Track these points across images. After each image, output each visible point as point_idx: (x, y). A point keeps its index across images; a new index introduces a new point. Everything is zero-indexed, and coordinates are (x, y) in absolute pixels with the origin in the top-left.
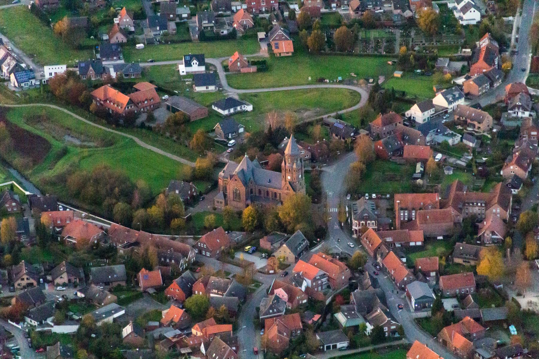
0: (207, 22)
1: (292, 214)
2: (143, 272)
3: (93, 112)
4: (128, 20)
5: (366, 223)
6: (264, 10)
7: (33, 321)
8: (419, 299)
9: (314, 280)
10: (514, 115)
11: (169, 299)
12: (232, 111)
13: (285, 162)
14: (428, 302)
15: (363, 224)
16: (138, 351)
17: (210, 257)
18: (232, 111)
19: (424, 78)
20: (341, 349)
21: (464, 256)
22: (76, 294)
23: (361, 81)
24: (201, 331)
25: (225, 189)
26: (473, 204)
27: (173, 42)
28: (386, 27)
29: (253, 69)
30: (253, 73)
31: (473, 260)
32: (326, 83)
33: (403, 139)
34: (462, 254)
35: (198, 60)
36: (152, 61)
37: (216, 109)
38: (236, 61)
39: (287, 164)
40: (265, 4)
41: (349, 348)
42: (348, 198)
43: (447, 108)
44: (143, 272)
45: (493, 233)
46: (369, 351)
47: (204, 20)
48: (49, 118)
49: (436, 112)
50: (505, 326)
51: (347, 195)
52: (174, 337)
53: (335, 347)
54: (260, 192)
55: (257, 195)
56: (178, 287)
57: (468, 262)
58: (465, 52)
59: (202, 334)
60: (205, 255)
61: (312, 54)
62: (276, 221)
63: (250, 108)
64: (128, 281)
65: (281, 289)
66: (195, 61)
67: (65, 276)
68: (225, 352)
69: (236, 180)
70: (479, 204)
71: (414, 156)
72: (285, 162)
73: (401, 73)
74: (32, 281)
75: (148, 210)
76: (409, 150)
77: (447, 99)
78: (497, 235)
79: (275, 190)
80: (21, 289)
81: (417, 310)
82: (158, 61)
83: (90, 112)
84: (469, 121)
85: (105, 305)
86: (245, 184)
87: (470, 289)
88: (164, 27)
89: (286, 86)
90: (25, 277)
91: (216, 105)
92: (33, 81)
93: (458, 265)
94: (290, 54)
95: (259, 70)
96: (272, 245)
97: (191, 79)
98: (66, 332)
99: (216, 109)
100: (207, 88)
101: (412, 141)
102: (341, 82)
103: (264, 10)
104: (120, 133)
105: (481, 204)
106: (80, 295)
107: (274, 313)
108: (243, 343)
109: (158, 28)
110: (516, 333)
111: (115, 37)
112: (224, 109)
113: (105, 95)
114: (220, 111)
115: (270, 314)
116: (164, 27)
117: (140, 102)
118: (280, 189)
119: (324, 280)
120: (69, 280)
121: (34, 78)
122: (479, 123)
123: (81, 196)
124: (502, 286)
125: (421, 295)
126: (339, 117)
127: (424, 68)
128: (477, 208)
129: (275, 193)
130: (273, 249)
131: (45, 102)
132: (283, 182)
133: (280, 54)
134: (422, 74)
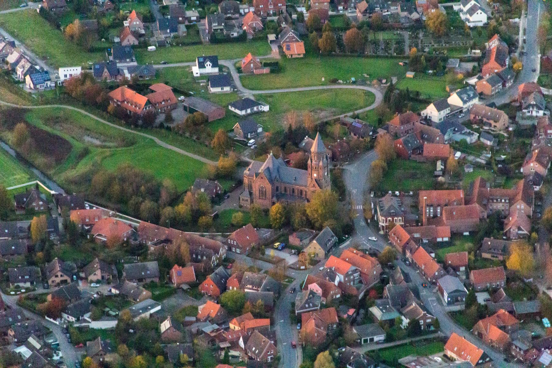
1: (320, 212)
3: (112, 113)
6: (271, 12)
7: (70, 317)
8: (451, 293)
9: (347, 275)
12: (249, 111)
13: (311, 160)
15: (389, 220)
18: (249, 111)
20: (378, 343)
22: (110, 291)
23: (375, 81)
24: (240, 326)
26: (497, 200)
27: (184, 44)
28: (394, 28)
29: (266, 70)
30: (267, 74)
31: (501, 254)
32: (340, 84)
33: (422, 138)
35: (211, 62)
36: (165, 63)
37: (233, 109)
39: (314, 162)
40: (272, 7)
41: (387, 341)
42: (372, 196)
43: (462, 108)
45: (519, 229)
47: (214, 22)
49: (451, 111)
50: (538, 319)
52: (213, 332)
53: (372, 340)
54: (285, 190)
57: (498, 257)
58: (475, 53)
59: (240, 328)
63: (266, 108)
64: (161, 277)
65: (315, 284)
66: (208, 63)
67: (99, 272)
69: (262, 178)
70: (503, 201)
71: (433, 154)
73: (413, 73)
74: (65, 278)
77: (462, 99)
78: (523, 230)
79: (302, 188)
81: (449, 303)
84: (485, 120)
85: (140, 301)
86: (271, 181)
87: (500, 282)
88: (174, 29)
90: (59, 274)
92: (49, 83)
93: (486, 260)
94: (302, 56)
95: (272, 72)
96: (301, 241)
98: (103, 328)
99: (233, 109)
102: (354, 83)
105: (505, 201)
107: (309, 307)
109: (168, 31)
112: (241, 110)
114: (238, 111)
115: (306, 308)
118: (306, 186)
119: (356, 275)
122: (495, 122)
126: (356, 117)
127: (435, 69)
128: (501, 204)
130: (302, 245)
131: (61, 104)
133: (292, 55)
134: (434, 74)
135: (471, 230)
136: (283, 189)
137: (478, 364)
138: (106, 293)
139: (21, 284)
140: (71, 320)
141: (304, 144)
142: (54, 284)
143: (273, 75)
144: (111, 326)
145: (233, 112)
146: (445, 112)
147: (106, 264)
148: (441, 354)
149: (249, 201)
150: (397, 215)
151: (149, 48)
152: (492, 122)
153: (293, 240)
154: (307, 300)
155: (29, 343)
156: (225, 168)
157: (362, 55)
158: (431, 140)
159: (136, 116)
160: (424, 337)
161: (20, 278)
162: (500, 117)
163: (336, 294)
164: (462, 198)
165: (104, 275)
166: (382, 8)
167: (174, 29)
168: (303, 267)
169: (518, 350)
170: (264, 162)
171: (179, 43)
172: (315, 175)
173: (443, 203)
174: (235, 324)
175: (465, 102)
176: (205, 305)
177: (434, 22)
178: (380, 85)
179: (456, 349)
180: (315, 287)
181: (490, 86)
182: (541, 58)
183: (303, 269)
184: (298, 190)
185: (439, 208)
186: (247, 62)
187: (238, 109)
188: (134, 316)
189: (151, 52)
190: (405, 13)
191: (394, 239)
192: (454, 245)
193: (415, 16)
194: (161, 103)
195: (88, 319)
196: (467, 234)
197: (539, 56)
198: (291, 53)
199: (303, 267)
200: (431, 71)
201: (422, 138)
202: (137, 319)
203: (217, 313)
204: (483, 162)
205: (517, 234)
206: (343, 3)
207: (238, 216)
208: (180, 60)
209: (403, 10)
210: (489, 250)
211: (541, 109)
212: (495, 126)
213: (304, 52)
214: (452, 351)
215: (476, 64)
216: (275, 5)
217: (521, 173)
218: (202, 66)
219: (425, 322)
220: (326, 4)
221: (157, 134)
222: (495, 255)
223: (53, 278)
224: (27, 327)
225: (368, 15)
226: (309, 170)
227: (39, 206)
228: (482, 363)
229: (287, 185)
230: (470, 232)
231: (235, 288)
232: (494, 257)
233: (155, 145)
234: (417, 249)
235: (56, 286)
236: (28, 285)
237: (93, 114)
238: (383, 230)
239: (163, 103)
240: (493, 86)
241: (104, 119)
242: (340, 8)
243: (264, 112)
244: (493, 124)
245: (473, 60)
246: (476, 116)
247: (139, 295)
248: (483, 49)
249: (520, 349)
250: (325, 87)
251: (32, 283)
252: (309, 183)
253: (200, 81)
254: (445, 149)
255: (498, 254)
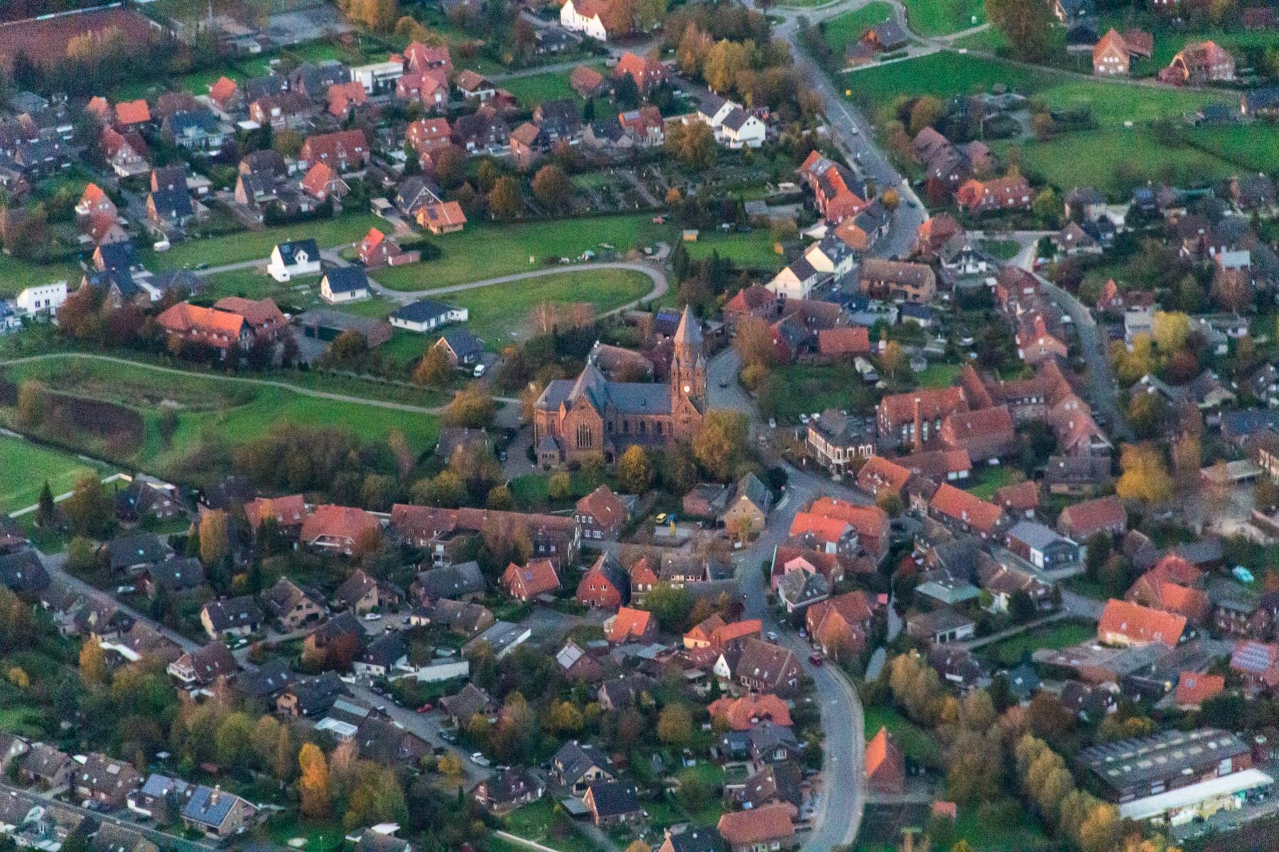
1: (726, 447)
2: (513, 571)
5: (857, 449)
6: (343, 166)
7: (374, 667)
12: (433, 323)
13: (678, 362)
17: (603, 539)
18: (433, 323)
20: (965, 639)
21: (1071, 478)
24: (708, 638)
26: (1022, 400)
28: (598, 168)
29: (413, 257)
30: (413, 264)
32: (563, 264)
34: (1066, 475)
35: (307, 251)
36: (205, 267)
37: (400, 323)
39: (682, 363)
40: (345, 155)
43: (832, 274)
44: (513, 571)
47: (257, 189)
48: (88, 374)
49: (819, 281)
50: (1223, 569)
53: (953, 636)
55: (621, 432)
59: (708, 644)
61: (506, 220)
62: (693, 466)
63: (462, 315)
66: (302, 253)
67: (374, 593)
68: (781, 660)
69: (582, 408)
70: (1034, 400)
72: (678, 362)
73: (696, 232)
74: (315, 609)
82: (215, 265)
84: (893, 286)
86: (601, 410)
88: (185, 209)
92: (10, 320)
94: (460, 228)
95: (425, 258)
98: (443, 678)
99: (400, 323)
100: (353, 294)
101: (826, 323)
102: (592, 259)
104: (241, 380)
107: (813, 596)
109: (174, 214)
110: (1251, 578)
111: (107, 235)
113: (185, 320)
114: (413, 326)
118: (669, 414)
120: (380, 601)
121: (11, 313)
122: (916, 287)
124: (1169, 514)
126: (640, 308)
128: (1030, 408)
131: (61, 350)
134: (736, 230)
135: (1001, 454)
136: (621, 423)
139: (236, 631)
142: (296, 623)
145: (402, 329)
146: (811, 281)
153: (692, 503)
154: (807, 584)
157: (569, 213)
159: (235, 350)
165: (382, 597)
166: (562, 133)
167: (185, 209)
172: (687, 389)
173: (932, 415)
174: (697, 637)
176: (615, 617)
177: (692, 141)
179: (1124, 626)
181: (864, 233)
182: (911, 185)
183: (739, 549)
188: (497, 651)
189: (161, 252)
191: (873, 482)
195: (406, 668)
197: (905, 182)
198: (440, 222)
200: (725, 226)
201: (807, 324)
202: (501, 656)
203: (989, 501)
212: (916, 296)
213: (464, 220)
214: (1117, 629)
216: (350, 152)
220: (443, 139)
224: (318, 685)
227: (164, 509)
228: (1185, 643)
229: (628, 417)
233: (297, 396)
234: (936, 489)
235: (299, 627)
236: (247, 630)
238: (839, 472)
239: (266, 326)
242: (470, 145)
243: (460, 322)
244: (910, 290)
246: (872, 281)
247: (476, 618)
249: (1238, 613)
250: (538, 273)
251: (254, 628)
252: (674, 405)
253: (299, 287)
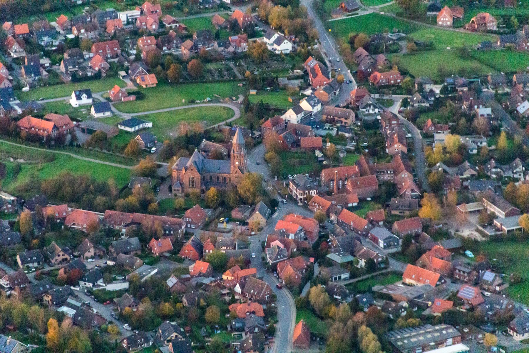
0: (72, 67)
1: (252, 190)
2: (153, 242)
3: (24, 138)
4: (4, 71)
5: (309, 193)
6: (109, 56)
7: (87, 284)
8: (386, 239)
9: (296, 234)
10: (367, 113)
11: (184, 260)
12: (137, 128)
14: (393, 241)
15: (306, 193)
16: (193, 293)
17: (196, 228)
18: (137, 128)
19: (273, 93)
20: (345, 279)
22: (106, 263)
23: (227, 99)
24: (233, 276)
25: (179, 179)
26: (384, 172)
27: (50, 84)
28: (218, 60)
29: (133, 98)
30: (133, 101)
31: (408, 210)
32: (197, 103)
33: (296, 134)
34: (398, 207)
37: (123, 128)
38: (118, 93)
39: (236, 152)
40: (110, 51)
41: (351, 277)
42: (276, 179)
44: (153, 242)
45: (413, 191)
46: (367, 279)
47: (69, 66)
50: (461, 252)
51: (274, 178)
52: (211, 282)
53: (340, 278)
54: (211, 177)
55: (209, 180)
56: (192, 248)
57: (404, 213)
58: (297, 72)
59: (233, 278)
60: (191, 228)
63: (150, 125)
64: (143, 251)
65: (277, 241)
66: (84, 95)
67: (92, 250)
68: (262, 288)
69: (192, 170)
70: (389, 172)
71: (310, 145)
74: (66, 256)
75: (126, 199)
76: (305, 142)
77: (310, 104)
78: (416, 192)
79: (225, 175)
80: (58, 264)
81: (385, 248)
82: (47, 99)
83: (22, 138)
84: (336, 118)
85: (137, 268)
87: (418, 230)
88: (37, 73)
89: (166, 108)
90: (61, 253)
91: (121, 124)
93: (395, 216)
94: (155, 85)
95: (138, 99)
96: (243, 214)
97: (85, 109)
98: (117, 289)
99: (123, 128)
102: (209, 102)
103: (109, 56)
104: (52, 151)
105: (391, 172)
106: (111, 263)
107: (281, 258)
108: (457, 218)
109: (33, 75)
110: (473, 256)
112: (131, 126)
114: (128, 129)
115: (278, 259)
116: (37, 73)
117: (65, 125)
118: (229, 174)
119: (302, 233)
120: (95, 254)
122: (346, 119)
123: (59, 197)
124: (441, 226)
125: (388, 236)
126: (227, 124)
127: (272, 86)
128: (387, 176)
129: (225, 178)
130: (244, 218)
132: (232, 167)
133: (147, 86)
134: (273, 91)
137: (437, 285)
138: (103, 265)
139: (31, 265)
140: (89, 286)
141: (203, 146)
143: (139, 102)
144: (120, 288)
146: (301, 115)
147: (96, 243)
148: (401, 282)
149: (180, 191)
150: (313, 189)
151: (24, 89)
152: (343, 120)
154: (278, 252)
155: (69, 303)
156: (148, 168)
158: (304, 135)
160: (380, 272)
161: (29, 259)
162: (349, 114)
163: (294, 248)
164: (357, 172)
168: (253, 233)
169: (462, 273)
170: (190, 158)
171: (47, 84)
172: (237, 163)
174: (228, 275)
175: (313, 107)
178: (231, 102)
179: (414, 276)
180: (276, 243)
182: (351, 72)
184: (222, 177)
185: (341, 182)
186: (116, 92)
187: (128, 126)
189: (26, 92)
190: (222, 48)
192: (362, 208)
193: (231, 49)
194: (63, 127)
195: (102, 284)
196: (369, 199)
197: (349, 71)
198: (147, 83)
199: (253, 233)
201: (296, 134)
204: (353, 148)
205: (411, 195)
206: (166, 45)
207: (180, 201)
208: (65, 94)
209: (220, 46)
210: (397, 208)
211: (376, 108)
212: (346, 123)
215: (302, 81)
216: (112, 49)
217: (388, 154)
218: (79, 98)
219: (377, 260)
220: (153, 46)
221: (69, 150)
222: (403, 211)
223: (57, 258)
225: (194, 51)
226: (232, 159)
229: (211, 174)
230: (371, 198)
231: (211, 251)
232: (401, 213)
236: (36, 264)
237: (6, 140)
238: (301, 202)
239: (64, 127)
240: (329, 93)
241: (19, 143)
243: (148, 128)
245: (298, 77)
248: (302, 68)
249: (464, 272)
251: (39, 264)
253: (82, 110)
254: (318, 141)
255: (405, 210)
